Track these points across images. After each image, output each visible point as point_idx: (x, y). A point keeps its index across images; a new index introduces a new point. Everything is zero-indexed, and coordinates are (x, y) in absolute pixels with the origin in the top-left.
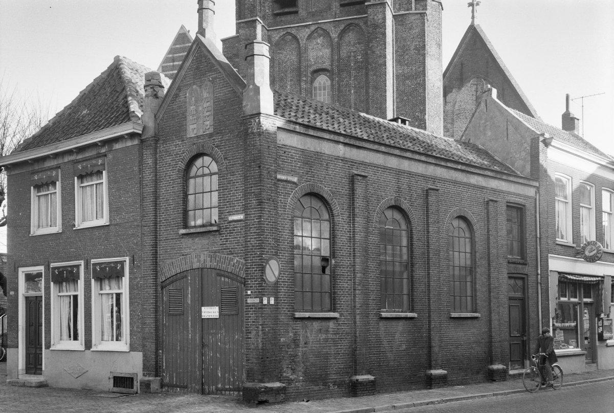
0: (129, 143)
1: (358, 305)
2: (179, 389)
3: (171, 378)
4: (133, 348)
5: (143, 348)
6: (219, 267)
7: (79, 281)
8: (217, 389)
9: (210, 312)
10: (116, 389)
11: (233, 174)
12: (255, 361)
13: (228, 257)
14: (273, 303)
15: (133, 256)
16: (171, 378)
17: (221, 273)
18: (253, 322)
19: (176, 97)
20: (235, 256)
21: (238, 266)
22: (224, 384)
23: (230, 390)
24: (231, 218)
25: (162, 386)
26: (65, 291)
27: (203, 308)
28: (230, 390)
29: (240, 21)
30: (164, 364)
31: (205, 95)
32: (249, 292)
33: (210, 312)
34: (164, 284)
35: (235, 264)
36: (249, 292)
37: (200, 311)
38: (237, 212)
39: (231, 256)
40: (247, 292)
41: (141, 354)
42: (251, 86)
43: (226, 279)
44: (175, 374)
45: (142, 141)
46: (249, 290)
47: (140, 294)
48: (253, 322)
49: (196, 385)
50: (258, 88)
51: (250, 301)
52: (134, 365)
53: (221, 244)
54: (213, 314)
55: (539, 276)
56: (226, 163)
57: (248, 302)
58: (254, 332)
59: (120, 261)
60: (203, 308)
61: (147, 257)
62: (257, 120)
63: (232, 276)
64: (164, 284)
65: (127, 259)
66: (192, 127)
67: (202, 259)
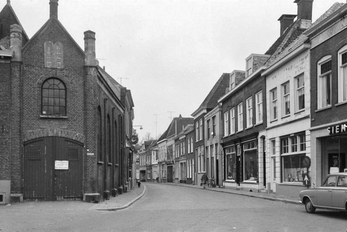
1: (324, 158)
6: (67, 137)
13: (73, 132)
15: (3, 125)
17: (67, 140)
20: (78, 132)
21: (80, 137)
29: (292, 167)
32: (88, 150)
34: (25, 143)
36: (88, 150)
39: (75, 132)
40: (87, 150)
45: (11, 62)
46: (88, 149)
47: (8, 148)
51: (88, 154)
53: (68, 126)
55: (181, 146)
57: (87, 155)
61: (14, 127)
63: (76, 142)
64: (25, 143)
66: (48, 62)
67: (55, 131)
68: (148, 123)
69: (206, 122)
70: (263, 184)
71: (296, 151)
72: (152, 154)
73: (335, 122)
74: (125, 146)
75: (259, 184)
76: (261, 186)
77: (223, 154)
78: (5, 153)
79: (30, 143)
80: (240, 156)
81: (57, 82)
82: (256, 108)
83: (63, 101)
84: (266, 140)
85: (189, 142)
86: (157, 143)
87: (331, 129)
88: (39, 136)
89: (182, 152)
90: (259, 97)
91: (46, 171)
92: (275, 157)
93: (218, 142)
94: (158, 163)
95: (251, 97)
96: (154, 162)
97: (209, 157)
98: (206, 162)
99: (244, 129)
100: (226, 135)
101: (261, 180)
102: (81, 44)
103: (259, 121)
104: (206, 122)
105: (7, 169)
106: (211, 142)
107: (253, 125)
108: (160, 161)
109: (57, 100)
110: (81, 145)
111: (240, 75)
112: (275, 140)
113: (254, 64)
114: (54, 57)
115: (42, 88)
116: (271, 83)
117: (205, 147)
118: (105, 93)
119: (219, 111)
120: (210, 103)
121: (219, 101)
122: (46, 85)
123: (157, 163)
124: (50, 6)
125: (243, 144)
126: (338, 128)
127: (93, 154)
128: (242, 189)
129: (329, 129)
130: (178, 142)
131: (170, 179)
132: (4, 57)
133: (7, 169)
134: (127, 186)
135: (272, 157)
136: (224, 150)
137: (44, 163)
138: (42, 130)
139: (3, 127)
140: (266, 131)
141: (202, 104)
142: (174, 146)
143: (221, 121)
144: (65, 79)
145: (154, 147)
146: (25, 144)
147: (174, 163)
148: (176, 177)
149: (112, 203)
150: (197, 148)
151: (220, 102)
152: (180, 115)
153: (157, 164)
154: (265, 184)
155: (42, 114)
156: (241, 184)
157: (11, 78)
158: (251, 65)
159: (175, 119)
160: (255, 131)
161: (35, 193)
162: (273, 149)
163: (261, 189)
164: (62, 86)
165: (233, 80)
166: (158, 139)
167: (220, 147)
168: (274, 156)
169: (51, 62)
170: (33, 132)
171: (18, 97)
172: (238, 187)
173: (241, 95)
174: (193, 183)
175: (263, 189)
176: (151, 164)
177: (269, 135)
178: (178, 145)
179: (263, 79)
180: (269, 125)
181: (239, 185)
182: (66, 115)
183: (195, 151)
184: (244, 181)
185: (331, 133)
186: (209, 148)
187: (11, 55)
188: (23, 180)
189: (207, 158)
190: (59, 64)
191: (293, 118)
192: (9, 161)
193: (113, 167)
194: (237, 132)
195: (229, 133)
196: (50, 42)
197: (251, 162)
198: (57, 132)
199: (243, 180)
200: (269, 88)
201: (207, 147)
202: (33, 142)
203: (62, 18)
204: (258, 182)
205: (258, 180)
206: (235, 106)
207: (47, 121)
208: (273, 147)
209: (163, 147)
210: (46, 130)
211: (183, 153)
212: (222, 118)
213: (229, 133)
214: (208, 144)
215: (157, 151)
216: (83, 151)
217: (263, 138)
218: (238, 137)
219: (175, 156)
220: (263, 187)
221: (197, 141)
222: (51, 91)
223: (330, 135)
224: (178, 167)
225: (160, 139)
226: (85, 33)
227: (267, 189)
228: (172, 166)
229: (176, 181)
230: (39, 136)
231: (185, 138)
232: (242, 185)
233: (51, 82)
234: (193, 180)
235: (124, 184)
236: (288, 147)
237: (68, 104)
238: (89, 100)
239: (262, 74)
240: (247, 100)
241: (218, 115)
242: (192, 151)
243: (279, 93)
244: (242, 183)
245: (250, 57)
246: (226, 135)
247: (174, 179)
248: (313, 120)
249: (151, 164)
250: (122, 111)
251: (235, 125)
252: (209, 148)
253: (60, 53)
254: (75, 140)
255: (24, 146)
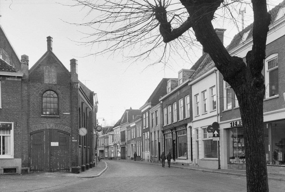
0: (16, 79)
2: (39, 171)
3: (35, 167)
4: (15, 157)
5: (22, 157)
7: (11, 130)
8: (57, 170)
9: (55, 144)
10: (5, 173)
11: (65, 99)
12: (75, 160)
13: (63, 126)
14: (58, 143)
16: (35, 167)
17: (59, 131)
18: (74, 147)
19: (38, 68)
22: (60, 168)
23: (63, 170)
24: (64, 114)
25: (30, 170)
26: (9, 133)
27: (51, 143)
28: (63, 170)
30: (31, 163)
31: (53, 70)
32: (73, 138)
33: (55, 144)
35: (66, 128)
36: (73, 138)
37: (50, 144)
38: (67, 112)
39: (65, 126)
41: (20, 159)
42: (74, 73)
43: (62, 133)
44: (37, 166)
45: (22, 80)
47: (20, 137)
48: (74, 147)
49: (47, 169)
50: (77, 75)
51: (73, 141)
52: (18, 163)
54: (56, 145)
56: (62, 95)
58: (75, 151)
59: (10, 124)
60: (51, 143)
61: (24, 123)
62: (77, 85)
63: (65, 133)
65: (13, 123)
66: (46, 80)
67: (51, 125)
68: (107, 115)
69: (150, 114)
70: (191, 160)
71: (206, 138)
72: (108, 138)
73: (234, 119)
74: (93, 133)
75: (188, 160)
76: (189, 161)
77: (163, 138)
78: (18, 140)
79: (34, 134)
80: (175, 140)
81: (52, 92)
82: (186, 107)
83: (56, 105)
84: (192, 129)
85: (138, 129)
86: (113, 129)
87: (231, 124)
88: (40, 129)
89: (132, 136)
90: (188, 99)
91: (45, 152)
92: (198, 141)
93: (160, 129)
94: (114, 144)
95: (182, 99)
96: (111, 143)
97: (153, 140)
98: (151, 144)
99: (177, 121)
100: (165, 124)
101: (189, 157)
102: (68, 67)
103: (188, 116)
104: (150, 114)
105: (20, 151)
106: (155, 129)
107: (184, 119)
108: (116, 143)
109: (52, 105)
110: (68, 135)
111: (174, 81)
112: (198, 129)
113: (184, 76)
114: (50, 77)
115: (42, 97)
116: (195, 90)
117: (150, 132)
118: (82, 99)
119: (160, 107)
120: (154, 100)
121: (160, 100)
122: (45, 95)
123: (113, 145)
124: (47, 42)
125: (177, 131)
126: (235, 123)
127: (76, 141)
128: (177, 163)
129: (230, 124)
130: (129, 129)
131: (123, 157)
132: (17, 76)
133: (20, 151)
134: (94, 162)
135: (197, 141)
136: (164, 135)
137: (44, 147)
138: (42, 124)
139: (16, 123)
140: (192, 123)
141: (147, 101)
142: (126, 132)
143: (162, 115)
144: (58, 91)
145: (110, 132)
146: (31, 134)
147: (127, 144)
148: (128, 155)
149: (89, 173)
150: (144, 134)
151: (161, 101)
152: (131, 107)
153: (113, 145)
154: (192, 160)
155: (42, 114)
156: (176, 160)
157: (22, 91)
158: (181, 77)
159: (127, 110)
160: (185, 123)
161: (37, 167)
162: (197, 135)
163: (190, 163)
164: (55, 95)
165: (169, 85)
166: (113, 126)
167: (161, 132)
168: (197, 140)
169: (48, 80)
170: (36, 126)
171: (26, 103)
172: (174, 162)
173: (175, 96)
174: (141, 160)
175: (191, 163)
176: (108, 145)
177: (194, 125)
178: (129, 130)
179: (190, 87)
180: (194, 119)
181: (175, 161)
182: (58, 115)
183: (143, 136)
184: (178, 158)
185: (231, 126)
186: (153, 134)
187: (22, 76)
188: (30, 158)
189: (152, 141)
190: (54, 81)
191: (209, 115)
192: (20, 146)
193: (82, 148)
194: (173, 123)
195: (168, 123)
196: (47, 66)
197: (184, 143)
198: (52, 126)
199: (177, 157)
200: (194, 94)
201: (151, 133)
202: (36, 133)
203: (54, 51)
204: (187, 158)
205: (187, 156)
206: (172, 104)
207: (46, 119)
208: (197, 134)
209: (118, 132)
210: (45, 125)
211: (133, 137)
212: (162, 111)
213: (168, 123)
214: (152, 131)
215: (113, 135)
216: (70, 138)
217: (191, 127)
218: (173, 126)
219: (127, 139)
220: (191, 161)
221: (144, 128)
222: (48, 99)
223: (231, 127)
224: (129, 148)
225: (116, 126)
226: (71, 60)
227: (193, 163)
228: (125, 147)
229: (128, 158)
230: (40, 129)
231: (135, 126)
232: (177, 161)
233: (48, 92)
234: (141, 157)
235: (93, 161)
236: (206, 134)
237: (60, 107)
238: (73, 105)
239: (189, 84)
240: (179, 101)
241: (159, 110)
242: (140, 136)
243: (200, 98)
244: (176, 159)
245: (181, 71)
246: (165, 124)
247: (126, 156)
248: (221, 117)
249: (108, 145)
250: (91, 109)
251: (172, 118)
252: (153, 134)
253: (54, 74)
254: (64, 131)
255: (30, 135)
